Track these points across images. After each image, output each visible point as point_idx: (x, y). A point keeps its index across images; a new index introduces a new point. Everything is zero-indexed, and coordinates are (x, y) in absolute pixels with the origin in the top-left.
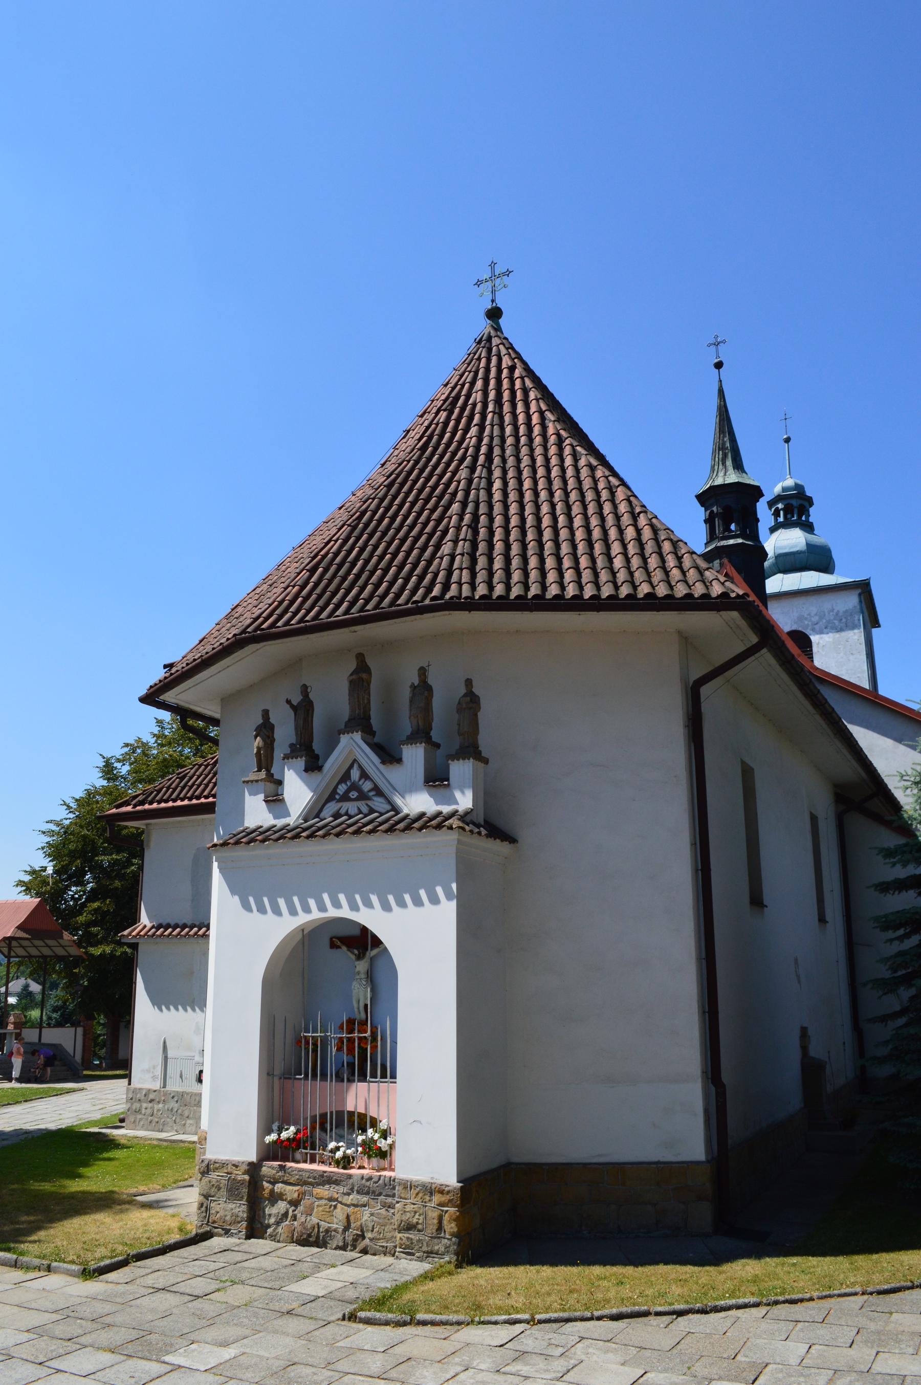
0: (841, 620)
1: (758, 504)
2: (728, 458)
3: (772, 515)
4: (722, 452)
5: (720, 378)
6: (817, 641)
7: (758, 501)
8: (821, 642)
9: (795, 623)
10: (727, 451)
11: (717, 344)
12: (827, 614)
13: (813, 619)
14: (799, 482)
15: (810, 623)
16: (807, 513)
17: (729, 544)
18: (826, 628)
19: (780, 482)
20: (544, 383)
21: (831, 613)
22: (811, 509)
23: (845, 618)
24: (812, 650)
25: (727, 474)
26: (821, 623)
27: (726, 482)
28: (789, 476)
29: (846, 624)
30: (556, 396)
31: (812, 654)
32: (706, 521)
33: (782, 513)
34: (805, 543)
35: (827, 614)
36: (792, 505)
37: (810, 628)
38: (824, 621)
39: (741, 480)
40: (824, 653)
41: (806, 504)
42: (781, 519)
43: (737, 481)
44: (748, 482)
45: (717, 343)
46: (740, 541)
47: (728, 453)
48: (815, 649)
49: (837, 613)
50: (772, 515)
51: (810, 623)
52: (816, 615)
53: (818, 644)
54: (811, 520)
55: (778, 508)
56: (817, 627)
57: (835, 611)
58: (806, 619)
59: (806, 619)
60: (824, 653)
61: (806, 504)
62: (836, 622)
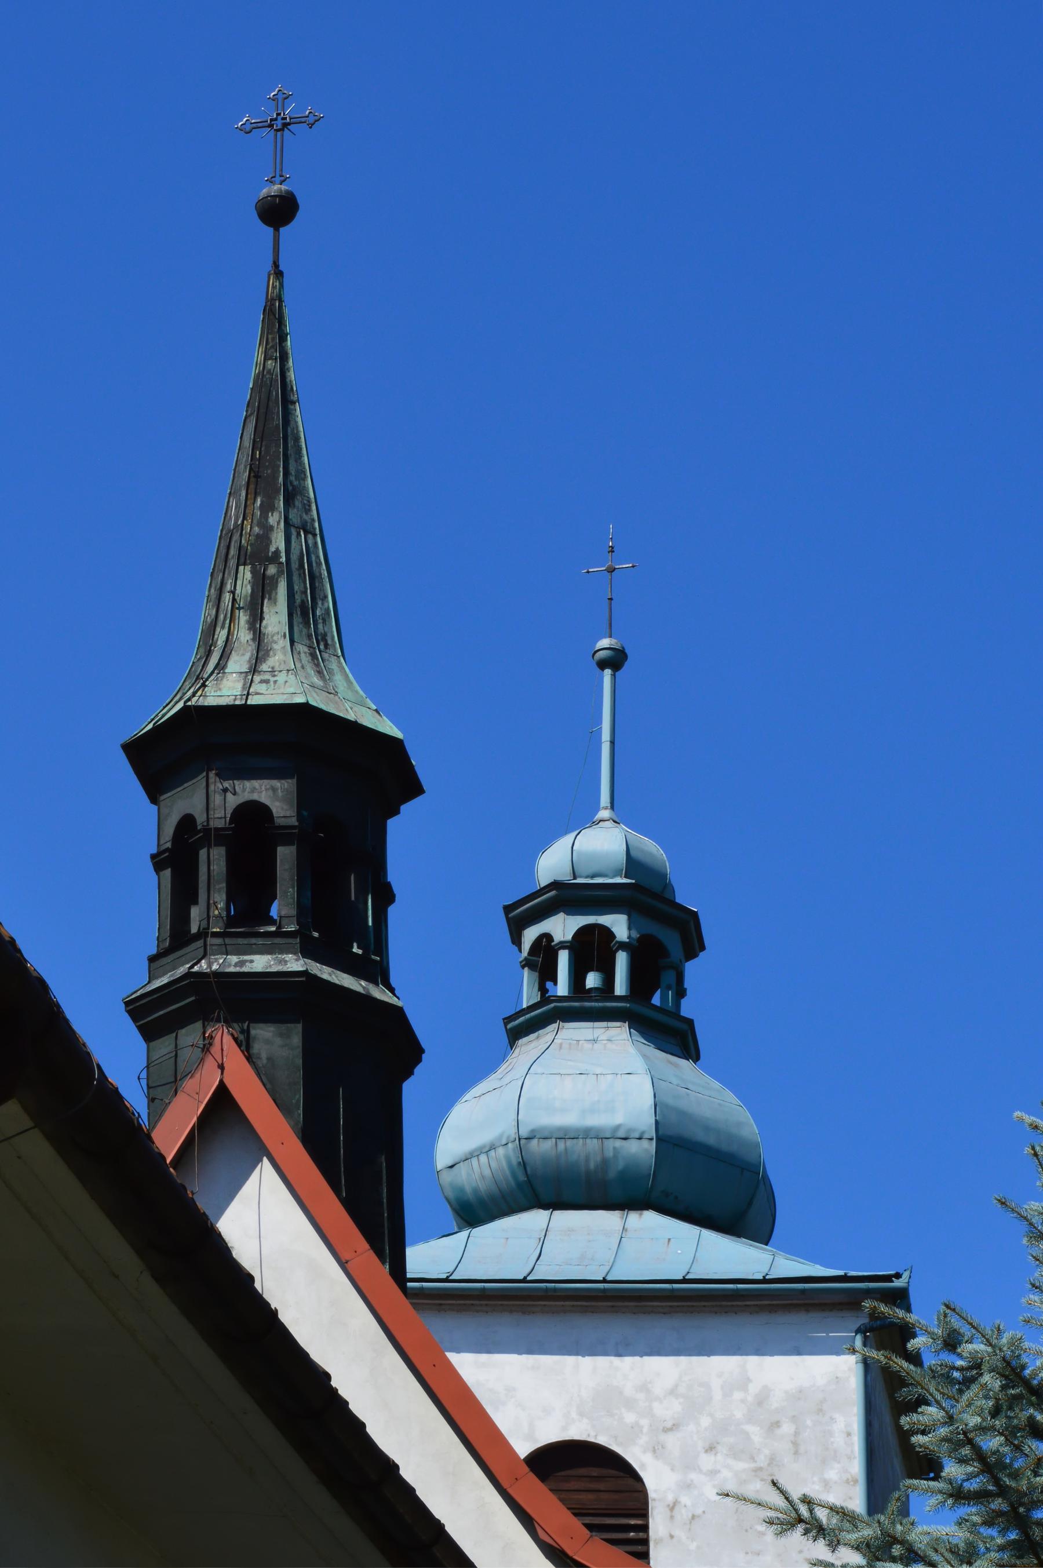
0: (777, 1424)
1: (392, 824)
2: (274, 601)
3: (527, 963)
4: (253, 572)
5: (276, 265)
6: (670, 1498)
7: (397, 812)
8: (685, 1500)
9: (581, 1414)
10: (272, 570)
11: (282, 126)
12: (717, 1395)
13: (658, 1409)
14: (651, 848)
15: (645, 1422)
16: (668, 977)
17: (245, 969)
18: (711, 1449)
19: (567, 832)
20: (437, 1517)
21: (738, 1395)
22: (692, 970)
23: (794, 1419)
24: (645, 1528)
25: (264, 667)
26: (692, 1427)
27: (253, 701)
28: (605, 814)
29: (795, 1444)
30: (76, 1025)
31: (645, 1542)
32: (159, 862)
33: (563, 958)
34: (650, 1101)
35: (717, 1395)
36: (607, 933)
37: (643, 1440)
38: (705, 1422)
39: (318, 701)
40: (693, 1546)
41: (671, 940)
42: (562, 987)
43: (300, 699)
44: (351, 716)
45: (278, 124)
46: (294, 964)
47: (274, 582)
48: (658, 1525)
49: (761, 1400)
50: (527, 963)
51: (645, 1422)
52: (673, 1392)
53: (672, 1507)
54: (687, 1009)
55: (547, 937)
56: (671, 1441)
57: (753, 1389)
58: (630, 1404)
59: (630, 1404)
60: (693, 1546)
61: (671, 940)
62: (756, 1433)
